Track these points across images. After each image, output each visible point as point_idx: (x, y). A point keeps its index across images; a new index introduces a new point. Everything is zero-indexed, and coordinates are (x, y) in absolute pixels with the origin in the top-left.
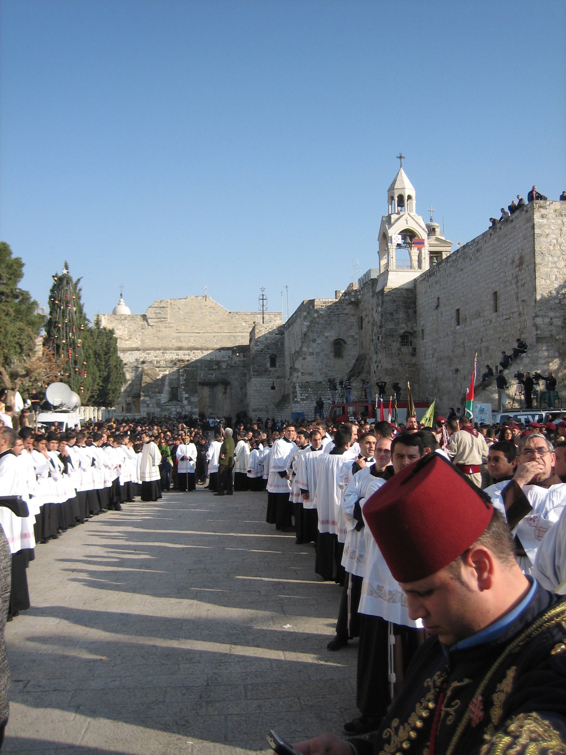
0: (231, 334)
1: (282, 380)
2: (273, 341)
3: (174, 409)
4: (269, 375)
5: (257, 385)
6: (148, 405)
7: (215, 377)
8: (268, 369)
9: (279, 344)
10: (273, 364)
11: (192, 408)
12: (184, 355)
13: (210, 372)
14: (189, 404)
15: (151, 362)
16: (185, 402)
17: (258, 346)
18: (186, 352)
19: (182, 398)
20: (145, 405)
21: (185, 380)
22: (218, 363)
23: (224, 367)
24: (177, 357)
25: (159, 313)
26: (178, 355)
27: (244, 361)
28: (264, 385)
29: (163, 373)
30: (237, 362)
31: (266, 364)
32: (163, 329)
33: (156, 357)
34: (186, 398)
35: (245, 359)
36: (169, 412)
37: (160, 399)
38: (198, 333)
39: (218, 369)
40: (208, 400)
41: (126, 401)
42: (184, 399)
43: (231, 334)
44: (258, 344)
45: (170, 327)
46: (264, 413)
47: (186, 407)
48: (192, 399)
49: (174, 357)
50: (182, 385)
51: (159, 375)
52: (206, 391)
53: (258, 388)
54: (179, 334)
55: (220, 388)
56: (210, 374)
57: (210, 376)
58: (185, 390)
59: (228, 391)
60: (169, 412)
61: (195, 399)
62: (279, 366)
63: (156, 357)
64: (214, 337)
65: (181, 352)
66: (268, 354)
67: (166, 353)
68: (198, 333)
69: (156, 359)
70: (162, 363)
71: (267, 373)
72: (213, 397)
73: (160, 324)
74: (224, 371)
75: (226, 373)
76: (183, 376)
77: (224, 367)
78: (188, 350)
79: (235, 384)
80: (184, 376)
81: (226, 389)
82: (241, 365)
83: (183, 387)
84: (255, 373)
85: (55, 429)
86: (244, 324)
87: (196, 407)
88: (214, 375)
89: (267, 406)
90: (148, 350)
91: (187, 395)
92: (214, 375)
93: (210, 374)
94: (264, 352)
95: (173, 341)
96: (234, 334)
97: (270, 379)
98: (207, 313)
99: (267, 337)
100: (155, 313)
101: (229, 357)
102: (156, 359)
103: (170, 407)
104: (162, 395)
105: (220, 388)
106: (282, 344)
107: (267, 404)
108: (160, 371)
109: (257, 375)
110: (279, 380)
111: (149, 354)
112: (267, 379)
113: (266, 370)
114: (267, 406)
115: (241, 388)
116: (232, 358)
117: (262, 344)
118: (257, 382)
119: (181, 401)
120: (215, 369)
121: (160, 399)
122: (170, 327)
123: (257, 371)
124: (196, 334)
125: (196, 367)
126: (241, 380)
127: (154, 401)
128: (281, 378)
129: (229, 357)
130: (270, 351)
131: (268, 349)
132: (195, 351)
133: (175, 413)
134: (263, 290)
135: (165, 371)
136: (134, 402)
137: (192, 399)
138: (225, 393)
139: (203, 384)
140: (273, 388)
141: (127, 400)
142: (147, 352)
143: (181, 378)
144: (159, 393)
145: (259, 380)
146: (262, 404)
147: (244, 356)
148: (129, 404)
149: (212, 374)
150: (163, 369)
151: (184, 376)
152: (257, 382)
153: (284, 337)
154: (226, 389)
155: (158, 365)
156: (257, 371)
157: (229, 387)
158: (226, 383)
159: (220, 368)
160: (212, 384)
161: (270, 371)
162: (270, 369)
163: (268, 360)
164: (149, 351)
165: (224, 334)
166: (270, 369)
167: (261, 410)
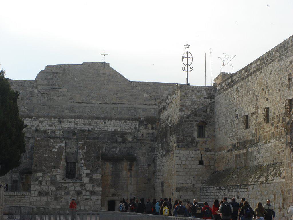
0: (132, 106)
1: (212, 153)
2: (202, 107)
3: (72, 188)
4: (196, 146)
5: (182, 159)
6: (41, 183)
7: (119, 151)
8: (195, 139)
9: (208, 110)
10: (201, 135)
11: (93, 187)
12: (84, 124)
13: (114, 145)
14: (90, 183)
15: (45, 132)
16: (86, 180)
17: (183, 111)
18: (87, 121)
19: (80, 175)
20: (37, 182)
21: (85, 153)
22: (123, 135)
23: (130, 139)
24: (76, 126)
25: (52, 79)
26: (77, 124)
27: (152, 134)
28: (190, 159)
29: (59, 144)
30: (145, 135)
31: (193, 133)
32: (55, 98)
33: (51, 126)
34: (87, 175)
35: (154, 131)
36: (66, 191)
37: (55, 176)
38: (94, 103)
39: (123, 143)
40: (110, 178)
41: (12, 177)
42: (85, 175)
43: (132, 106)
44: (184, 109)
45: (64, 96)
46: (190, 193)
47: (87, 186)
48: (95, 176)
49: (72, 126)
50: (82, 159)
51: (54, 147)
52: (109, 167)
53: (184, 163)
54: (73, 104)
55: (125, 165)
56: (114, 148)
57: (114, 150)
58: (85, 165)
59: (134, 168)
60: (66, 191)
61: (97, 176)
62: (208, 136)
63: (51, 126)
64: (113, 108)
65: (80, 121)
66: (196, 121)
67: (63, 122)
68: (94, 103)
69: (51, 128)
70: (58, 133)
71: (194, 145)
72: (116, 174)
73: (52, 92)
74: (129, 145)
75: (132, 147)
76: (82, 148)
77: (130, 139)
78: (89, 119)
79: (143, 160)
80: (84, 148)
81: (131, 165)
82: (149, 138)
83: (83, 162)
84: (180, 144)
85: (81, 158)
86: (145, 95)
87: (99, 186)
88: (118, 149)
89: (193, 185)
90: (42, 117)
91: (88, 171)
92: (118, 149)
93: (114, 148)
94: (190, 119)
95: (66, 111)
96: (135, 106)
97: (198, 152)
98: (106, 82)
99: (194, 102)
100: (46, 79)
101: (136, 128)
102: (51, 128)
103: (67, 185)
104: (59, 170)
105: (125, 165)
106: (212, 111)
107: (194, 182)
108: (54, 142)
109: (182, 147)
110: (208, 153)
111: (42, 122)
112: (194, 152)
113: (193, 141)
114: (193, 185)
115: (149, 165)
116: (139, 130)
117: (188, 109)
118: (182, 155)
119: (80, 178)
120: (120, 142)
121: (55, 176)
122: (64, 96)
123: (183, 142)
124: (93, 105)
125: (98, 138)
126: (148, 155)
127: (48, 178)
128: (210, 151)
129: (136, 128)
130: (197, 118)
131: (196, 115)
132: (96, 121)
133: (74, 192)
134: (187, 46)
135: (61, 142)
136: (22, 179)
137: (95, 176)
138: (130, 170)
139: (105, 158)
140: (201, 163)
141: (13, 177)
142: (40, 119)
143: (81, 151)
144: (55, 167)
145: (184, 152)
146: (187, 181)
147: (153, 128)
148: (15, 182)
149: (116, 148)
150: (58, 140)
151: (84, 148)
152: (182, 155)
153: (214, 102)
154: (131, 165)
155: (53, 135)
156: (183, 142)
157: (135, 163)
158: (132, 159)
159: (125, 140)
160: (115, 160)
161: (197, 142)
162: (197, 139)
163: (196, 128)
164: (43, 119)
165: (124, 106)
166: (197, 139)
167: (186, 190)
